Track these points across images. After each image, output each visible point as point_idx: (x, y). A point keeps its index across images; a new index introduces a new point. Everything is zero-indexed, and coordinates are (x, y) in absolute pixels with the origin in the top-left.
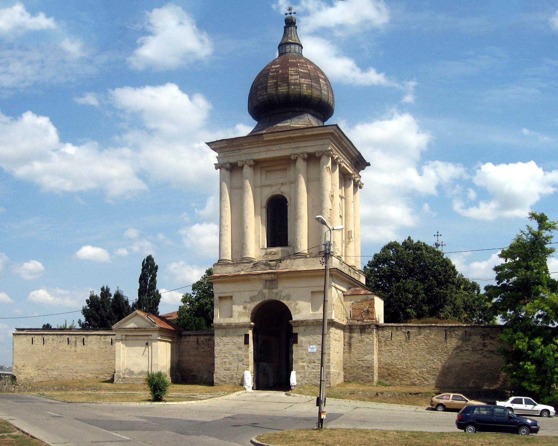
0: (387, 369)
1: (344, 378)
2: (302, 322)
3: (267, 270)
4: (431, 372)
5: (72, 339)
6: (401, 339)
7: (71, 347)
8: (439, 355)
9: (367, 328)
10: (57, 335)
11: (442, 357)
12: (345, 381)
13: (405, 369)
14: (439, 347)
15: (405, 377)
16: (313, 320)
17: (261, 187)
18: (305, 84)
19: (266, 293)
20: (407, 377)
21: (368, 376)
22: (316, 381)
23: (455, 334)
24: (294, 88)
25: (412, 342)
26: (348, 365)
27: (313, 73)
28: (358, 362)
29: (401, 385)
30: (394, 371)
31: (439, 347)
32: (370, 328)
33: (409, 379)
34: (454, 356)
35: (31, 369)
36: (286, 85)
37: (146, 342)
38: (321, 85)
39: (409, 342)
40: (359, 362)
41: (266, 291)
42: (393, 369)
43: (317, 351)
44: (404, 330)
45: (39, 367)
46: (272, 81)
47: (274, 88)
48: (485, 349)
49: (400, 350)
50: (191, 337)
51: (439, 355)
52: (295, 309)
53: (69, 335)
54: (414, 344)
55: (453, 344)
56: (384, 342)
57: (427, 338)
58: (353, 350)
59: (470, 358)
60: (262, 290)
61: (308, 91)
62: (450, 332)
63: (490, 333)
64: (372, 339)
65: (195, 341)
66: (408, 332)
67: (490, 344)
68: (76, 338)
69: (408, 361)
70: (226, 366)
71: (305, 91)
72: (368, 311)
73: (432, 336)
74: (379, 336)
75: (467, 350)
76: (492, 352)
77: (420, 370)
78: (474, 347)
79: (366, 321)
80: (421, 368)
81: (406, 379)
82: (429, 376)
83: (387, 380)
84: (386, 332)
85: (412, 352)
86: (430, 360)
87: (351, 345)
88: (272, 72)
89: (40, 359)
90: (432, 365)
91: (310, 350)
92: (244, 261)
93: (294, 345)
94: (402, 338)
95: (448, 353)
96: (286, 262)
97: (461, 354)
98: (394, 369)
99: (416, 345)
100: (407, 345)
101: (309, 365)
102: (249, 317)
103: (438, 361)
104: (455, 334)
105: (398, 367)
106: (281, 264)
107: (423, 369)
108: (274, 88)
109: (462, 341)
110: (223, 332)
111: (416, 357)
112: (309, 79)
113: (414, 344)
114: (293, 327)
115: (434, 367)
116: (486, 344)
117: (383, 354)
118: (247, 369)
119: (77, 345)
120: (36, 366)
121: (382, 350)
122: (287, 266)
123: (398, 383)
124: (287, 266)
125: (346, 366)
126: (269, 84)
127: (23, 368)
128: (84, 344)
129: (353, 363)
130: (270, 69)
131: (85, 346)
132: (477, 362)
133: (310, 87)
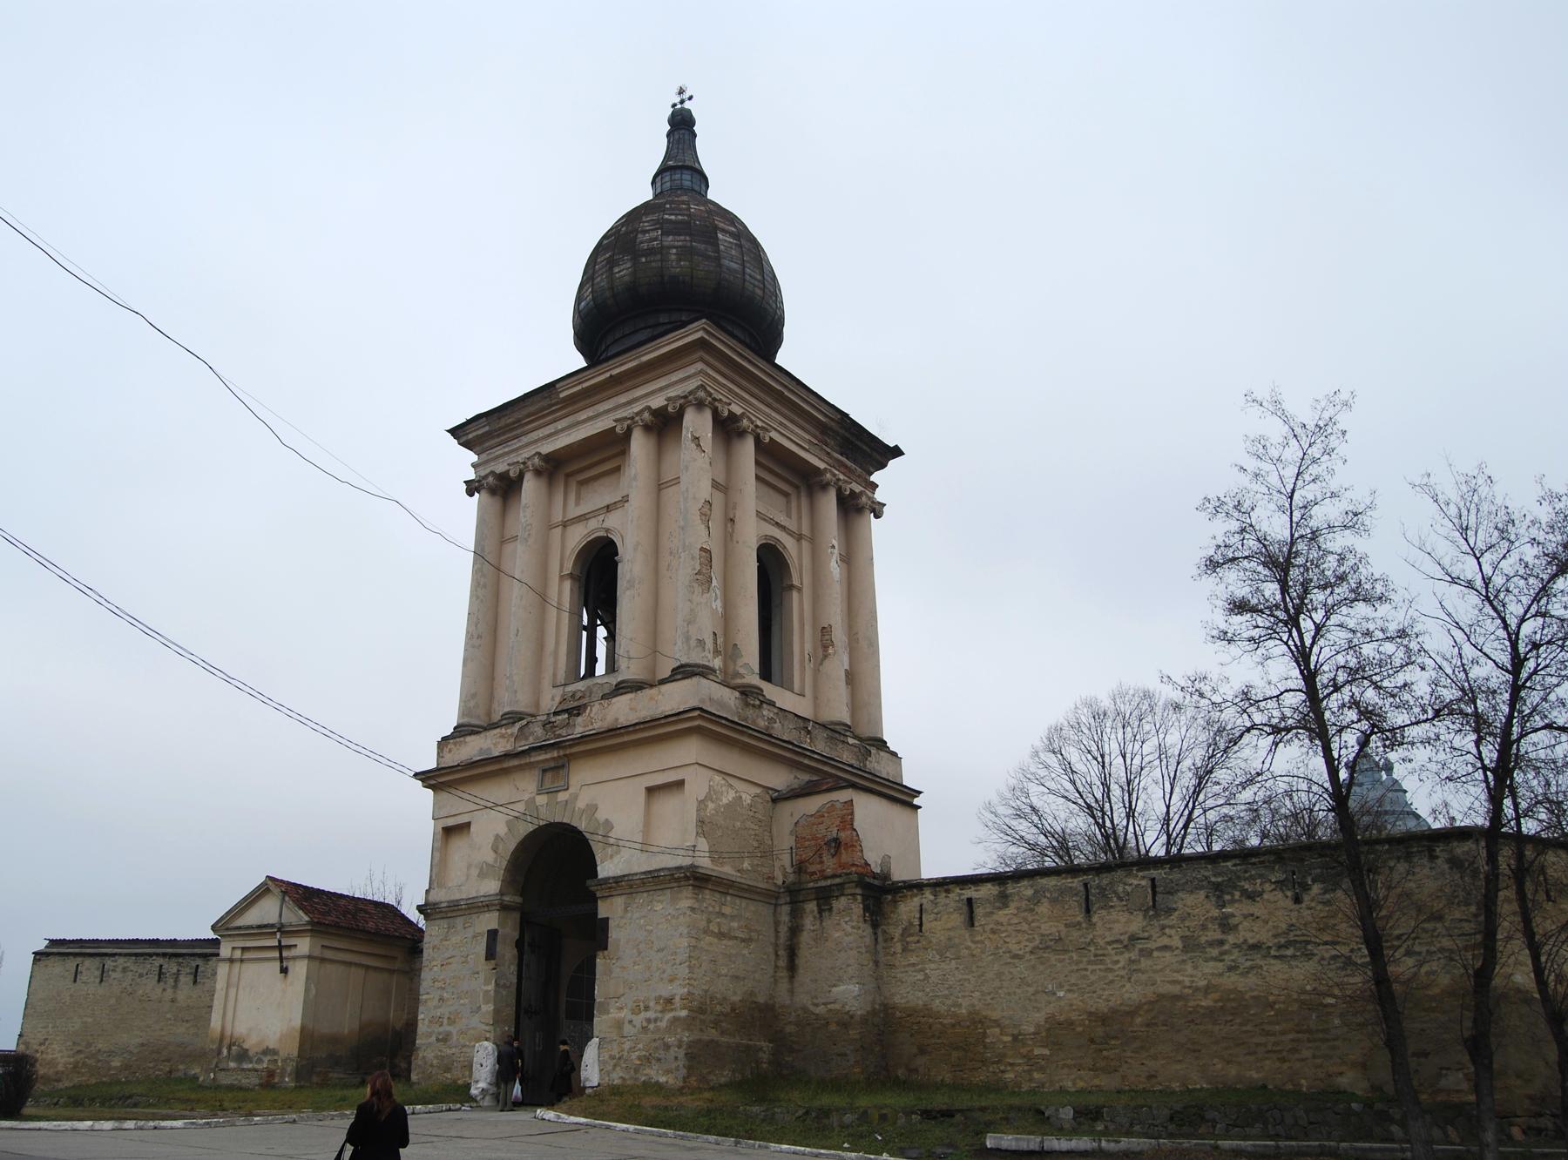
5: (171, 967)
7: (164, 990)
9: (837, 897)
16: (644, 873)
17: (565, 526)
18: (675, 247)
19: (542, 806)
27: (700, 221)
35: (60, 1051)
38: (722, 247)
41: (542, 800)
45: (79, 1044)
48: (1231, 939)
53: (164, 955)
56: (900, 941)
59: (1181, 978)
60: (534, 798)
63: (1239, 878)
67: (1245, 917)
68: (179, 964)
71: (676, 266)
75: (1165, 948)
76: (1256, 947)
78: (1188, 934)
89: (86, 1023)
96: (591, 710)
97: (1145, 963)
106: (580, 719)
108: (606, 271)
109: (1145, 917)
112: (686, 234)
114: (599, 901)
116: (1233, 921)
119: (180, 984)
120: (74, 1043)
122: (592, 724)
127: (43, 1048)
128: (195, 982)
131: (199, 986)
132: (1207, 990)
133: (687, 252)
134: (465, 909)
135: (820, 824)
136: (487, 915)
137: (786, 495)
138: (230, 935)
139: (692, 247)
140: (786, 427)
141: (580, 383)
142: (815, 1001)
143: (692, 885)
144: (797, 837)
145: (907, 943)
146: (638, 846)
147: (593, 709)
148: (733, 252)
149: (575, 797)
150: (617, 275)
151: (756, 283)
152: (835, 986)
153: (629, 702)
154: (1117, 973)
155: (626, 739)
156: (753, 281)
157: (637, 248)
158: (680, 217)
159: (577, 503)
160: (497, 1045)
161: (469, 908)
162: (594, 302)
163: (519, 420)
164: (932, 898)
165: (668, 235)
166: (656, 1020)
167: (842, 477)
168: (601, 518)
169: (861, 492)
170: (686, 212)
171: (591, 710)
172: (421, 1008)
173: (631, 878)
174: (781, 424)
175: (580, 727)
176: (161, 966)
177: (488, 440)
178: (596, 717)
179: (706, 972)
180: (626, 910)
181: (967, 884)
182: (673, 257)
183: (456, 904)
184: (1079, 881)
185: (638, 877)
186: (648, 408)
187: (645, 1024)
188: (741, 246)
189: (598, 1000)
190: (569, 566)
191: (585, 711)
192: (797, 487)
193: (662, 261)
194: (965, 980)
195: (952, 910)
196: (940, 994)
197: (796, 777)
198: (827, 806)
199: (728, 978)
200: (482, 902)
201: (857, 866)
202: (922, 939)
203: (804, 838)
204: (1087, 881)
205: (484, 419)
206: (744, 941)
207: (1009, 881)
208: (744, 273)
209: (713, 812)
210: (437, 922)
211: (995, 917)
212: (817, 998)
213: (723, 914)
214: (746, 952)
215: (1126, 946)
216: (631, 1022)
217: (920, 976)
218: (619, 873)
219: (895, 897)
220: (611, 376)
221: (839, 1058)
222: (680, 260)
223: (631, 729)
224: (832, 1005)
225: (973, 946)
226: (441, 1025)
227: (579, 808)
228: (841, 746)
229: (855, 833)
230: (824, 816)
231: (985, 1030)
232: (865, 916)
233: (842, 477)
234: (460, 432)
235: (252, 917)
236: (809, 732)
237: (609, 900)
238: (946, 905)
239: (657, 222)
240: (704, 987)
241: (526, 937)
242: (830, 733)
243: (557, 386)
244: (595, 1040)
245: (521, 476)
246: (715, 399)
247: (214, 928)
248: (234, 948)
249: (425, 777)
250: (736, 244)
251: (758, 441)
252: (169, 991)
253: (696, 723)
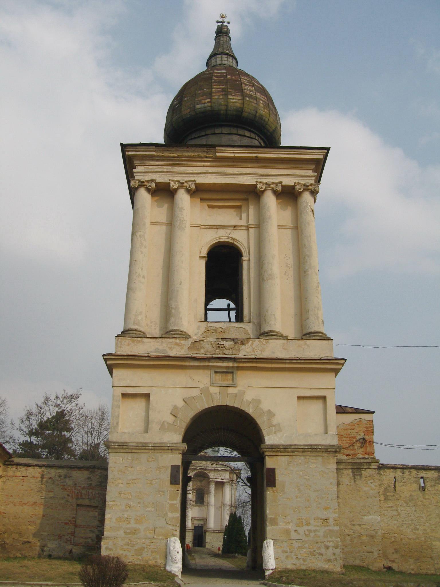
3: (217, 354)
19: (216, 394)
36: (239, 94)
41: (215, 390)
46: (218, 87)
47: (222, 95)
50: (31, 469)
52: (271, 425)
60: (208, 388)
65: (37, 478)
70: (128, 526)
72: (364, 439)
79: (361, 456)
88: (217, 76)
92: (175, 336)
93: (270, 489)
96: (253, 344)
101: (298, 528)
102: (180, 434)
106: (243, 347)
110: (127, 459)
124: (254, 351)
126: (214, 90)
130: (213, 73)
134: (151, 449)
135: (352, 429)
136: (170, 455)
142: (353, 523)
145: (387, 496)
147: (254, 343)
152: (365, 515)
155: (287, 366)
158: (258, 85)
161: (154, 449)
164: (401, 474)
166: (315, 531)
168: (229, 231)
173: (296, 447)
177: (148, 160)
178: (257, 348)
183: (144, 445)
185: (302, 447)
189: (269, 517)
191: (248, 343)
195: (412, 482)
196: (406, 523)
198: (357, 421)
200: (168, 447)
202: (395, 494)
203: (342, 435)
211: (436, 488)
212: (354, 522)
216: (296, 531)
217: (395, 513)
219: (380, 472)
221: (368, 554)
223: (294, 361)
224: (364, 526)
225: (425, 501)
226: (129, 523)
227: (247, 400)
230: (355, 426)
231: (432, 542)
238: (409, 479)
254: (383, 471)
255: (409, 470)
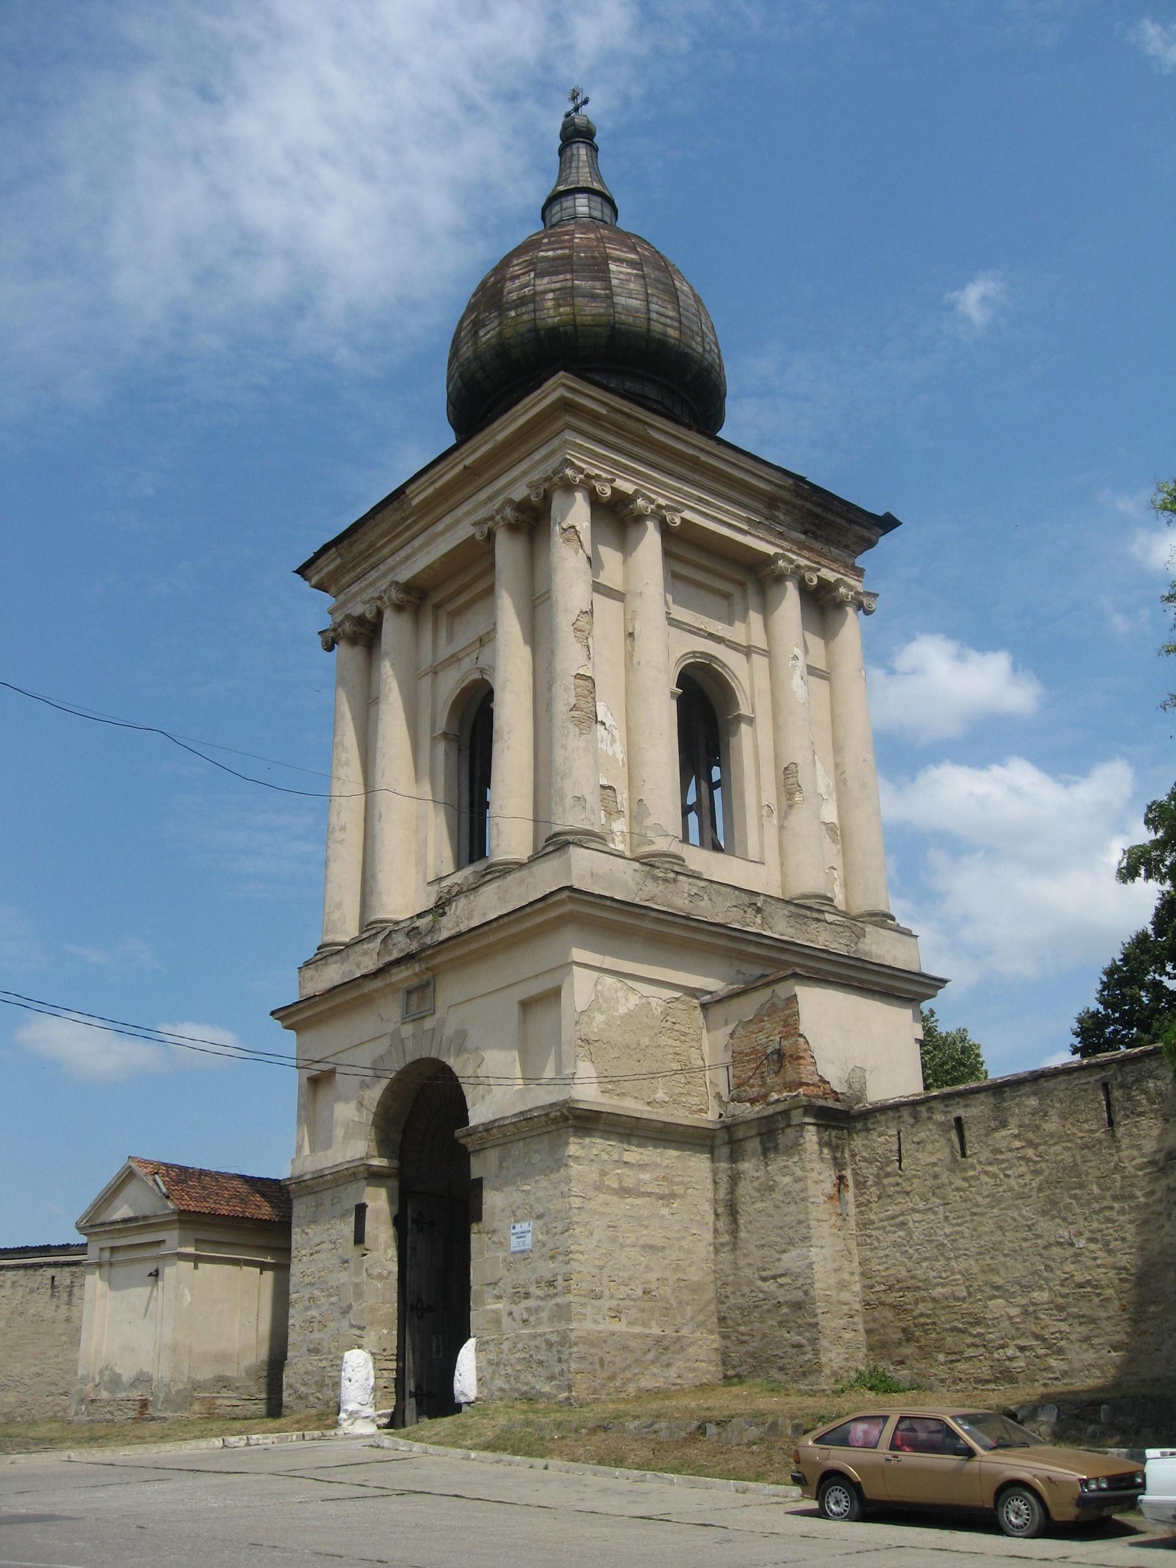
0: (897, 1308)
1: (724, 1363)
2: (488, 1130)
4: (1069, 1305)
6: (933, 1159)
7: (58, 1306)
8: (1095, 1212)
9: (783, 1129)
10: (25, 1267)
11: (1108, 1220)
12: (725, 1377)
13: (964, 1300)
14: (1087, 1174)
15: (969, 1340)
17: (435, 673)
20: (977, 1341)
21: (799, 1346)
22: (530, 1378)
23: (1145, 1092)
24: (517, 315)
25: (979, 1168)
26: (732, 1301)
27: (584, 252)
28: (760, 1283)
29: (954, 1382)
30: (921, 1315)
31: (1087, 1174)
32: (789, 1126)
33: (982, 1350)
34: (1160, 1208)
37: (151, 1268)
38: (614, 282)
39: (965, 1170)
40: (765, 1286)
41: (408, 1030)
42: (916, 1303)
43: (534, 1245)
44: (939, 1117)
49: (936, 1213)
51: (1095, 1212)
53: (56, 1265)
54: (987, 1173)
55: (1149, 1146)
56: (876, 1184)
57: (1030, 1135)
58: (743, 1234)
61: (562, 310)
62: (1122, 1086)
64: (799, 1173)
66: (958, 1120)
68: (73, 1274)
69: (972, 1262)
71: (552, 313)
72: (779, 1053)
73: (1052, 1125)
74: (858, 1158)
77: (1025, 1301)
80: (1026, 1288)
81: (971, 1352)
82: (1064, 1327)
83: (901, 1363)
84: (880, 1136)
85: (981, 1214)
86: (1060, 1244)
87: (737, 1212)
90: (1070, 1267)
91: (515, 1244)
94: (939, 1155)
95: (1133, 1197)
96: (457, 906)
98: (921, 1306)
99: (995, 1176)
100: (959, 1183)
103: (1093, 1246)
104: (1145, 1092)
105: (938, 1292)
106: (444, 920)
107: (1035, 1294)
111: (998, 1236)
112: (565, 272)
113: (987, 1173)
115: (1079, 1278)
117: (878, 1239)
118: (360, 1341)
121: (872, 1222)
123: (941, 1371)
125: (724, 1307)
129: (746, 1290)
133: (567, 295)
137: (727, 596)
138: (96, 1233)
139: (573, 288)
140: (708, 503)
141: (432, 483)
143: (572, 1126)
144: (733, 1052)
146: (294, 1063)
148: (632, 286)
149: (442, 1023)
150: (483, 339)
151: (668, 321)
152: (784, 1251)
153: (496, 890)
154: (1153, 1208)
156: (663, 320)
157: (504, 300)
158: (559, 252)
159: (450, 640)
160: (373, 1354)
162: (462, 381)
163: (372, 545)
165: (543, 277)
167: (803, 562)
169: (838, 581)
170: (568, 244)
171: (457, 906)
172: (292, 1311)
174: (700, 500)
175: (448, 927)
176: (53, 1278)
179: (599, 1241)
180: (500, 1167)
181: (954, 1099)
182: (550, 304)
184: (1096, 1081)
186: (510, 501)
187: (525, 1316)
188: (643, 277)
190: (442, 723)
192: (742, 585)
193: (535, 311)
194: (957, 1233)
197: (739, 972)
199: (637, 1249)
200: (347, 1169)
201: (807, 1084)
204: (1105, 1081)
205: (334, 549)
206: (662, 1199)
207: (1007, 1089)
208: (649, 311)
209: (602, 1026)
210: (305, 1199)
212: (764, 1270)
213: (626, 1163)
214: (665, 1211)
215: (1162, 1170)
218: (491, 1117)
220: (465, 467)
222: (560, 306)
228: (814, 925)
229: (802, 1040)
232: (821, 1152)
233: (803, 562)
234: (308, 572)
235: (122, 1211)
236: (759, 910)
237: (482, 1155)
239: (530, 263)
240: (597, 1262)
241: (409, 1211)
242: (792, 908)
243: (408, 491)
244: (471, 1344)
245: (380, 614)
246: (588, 477)
247: (80, 1229)
248: (102, 1249)
249: (282, 1014)
250: (636, 275)
251: (666, 531)
252: (64, 1308)
253: (569, 907)
254: (872, 1120)
255: (927, 1104)
